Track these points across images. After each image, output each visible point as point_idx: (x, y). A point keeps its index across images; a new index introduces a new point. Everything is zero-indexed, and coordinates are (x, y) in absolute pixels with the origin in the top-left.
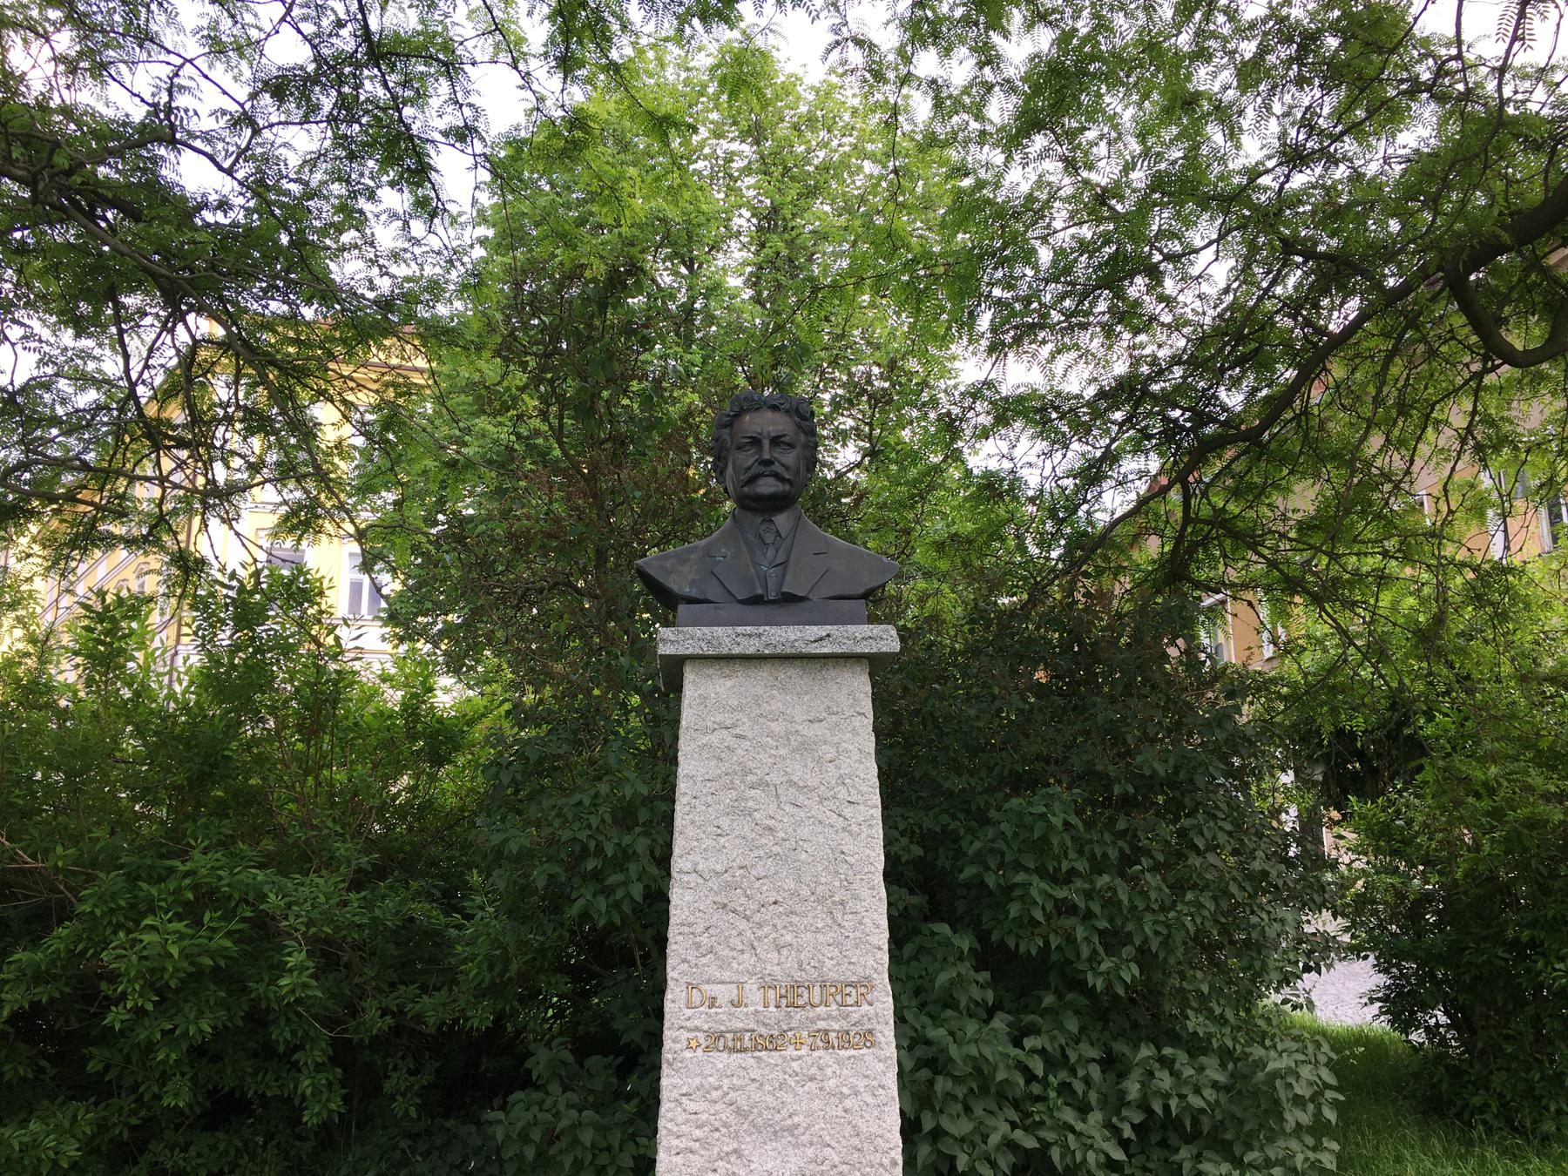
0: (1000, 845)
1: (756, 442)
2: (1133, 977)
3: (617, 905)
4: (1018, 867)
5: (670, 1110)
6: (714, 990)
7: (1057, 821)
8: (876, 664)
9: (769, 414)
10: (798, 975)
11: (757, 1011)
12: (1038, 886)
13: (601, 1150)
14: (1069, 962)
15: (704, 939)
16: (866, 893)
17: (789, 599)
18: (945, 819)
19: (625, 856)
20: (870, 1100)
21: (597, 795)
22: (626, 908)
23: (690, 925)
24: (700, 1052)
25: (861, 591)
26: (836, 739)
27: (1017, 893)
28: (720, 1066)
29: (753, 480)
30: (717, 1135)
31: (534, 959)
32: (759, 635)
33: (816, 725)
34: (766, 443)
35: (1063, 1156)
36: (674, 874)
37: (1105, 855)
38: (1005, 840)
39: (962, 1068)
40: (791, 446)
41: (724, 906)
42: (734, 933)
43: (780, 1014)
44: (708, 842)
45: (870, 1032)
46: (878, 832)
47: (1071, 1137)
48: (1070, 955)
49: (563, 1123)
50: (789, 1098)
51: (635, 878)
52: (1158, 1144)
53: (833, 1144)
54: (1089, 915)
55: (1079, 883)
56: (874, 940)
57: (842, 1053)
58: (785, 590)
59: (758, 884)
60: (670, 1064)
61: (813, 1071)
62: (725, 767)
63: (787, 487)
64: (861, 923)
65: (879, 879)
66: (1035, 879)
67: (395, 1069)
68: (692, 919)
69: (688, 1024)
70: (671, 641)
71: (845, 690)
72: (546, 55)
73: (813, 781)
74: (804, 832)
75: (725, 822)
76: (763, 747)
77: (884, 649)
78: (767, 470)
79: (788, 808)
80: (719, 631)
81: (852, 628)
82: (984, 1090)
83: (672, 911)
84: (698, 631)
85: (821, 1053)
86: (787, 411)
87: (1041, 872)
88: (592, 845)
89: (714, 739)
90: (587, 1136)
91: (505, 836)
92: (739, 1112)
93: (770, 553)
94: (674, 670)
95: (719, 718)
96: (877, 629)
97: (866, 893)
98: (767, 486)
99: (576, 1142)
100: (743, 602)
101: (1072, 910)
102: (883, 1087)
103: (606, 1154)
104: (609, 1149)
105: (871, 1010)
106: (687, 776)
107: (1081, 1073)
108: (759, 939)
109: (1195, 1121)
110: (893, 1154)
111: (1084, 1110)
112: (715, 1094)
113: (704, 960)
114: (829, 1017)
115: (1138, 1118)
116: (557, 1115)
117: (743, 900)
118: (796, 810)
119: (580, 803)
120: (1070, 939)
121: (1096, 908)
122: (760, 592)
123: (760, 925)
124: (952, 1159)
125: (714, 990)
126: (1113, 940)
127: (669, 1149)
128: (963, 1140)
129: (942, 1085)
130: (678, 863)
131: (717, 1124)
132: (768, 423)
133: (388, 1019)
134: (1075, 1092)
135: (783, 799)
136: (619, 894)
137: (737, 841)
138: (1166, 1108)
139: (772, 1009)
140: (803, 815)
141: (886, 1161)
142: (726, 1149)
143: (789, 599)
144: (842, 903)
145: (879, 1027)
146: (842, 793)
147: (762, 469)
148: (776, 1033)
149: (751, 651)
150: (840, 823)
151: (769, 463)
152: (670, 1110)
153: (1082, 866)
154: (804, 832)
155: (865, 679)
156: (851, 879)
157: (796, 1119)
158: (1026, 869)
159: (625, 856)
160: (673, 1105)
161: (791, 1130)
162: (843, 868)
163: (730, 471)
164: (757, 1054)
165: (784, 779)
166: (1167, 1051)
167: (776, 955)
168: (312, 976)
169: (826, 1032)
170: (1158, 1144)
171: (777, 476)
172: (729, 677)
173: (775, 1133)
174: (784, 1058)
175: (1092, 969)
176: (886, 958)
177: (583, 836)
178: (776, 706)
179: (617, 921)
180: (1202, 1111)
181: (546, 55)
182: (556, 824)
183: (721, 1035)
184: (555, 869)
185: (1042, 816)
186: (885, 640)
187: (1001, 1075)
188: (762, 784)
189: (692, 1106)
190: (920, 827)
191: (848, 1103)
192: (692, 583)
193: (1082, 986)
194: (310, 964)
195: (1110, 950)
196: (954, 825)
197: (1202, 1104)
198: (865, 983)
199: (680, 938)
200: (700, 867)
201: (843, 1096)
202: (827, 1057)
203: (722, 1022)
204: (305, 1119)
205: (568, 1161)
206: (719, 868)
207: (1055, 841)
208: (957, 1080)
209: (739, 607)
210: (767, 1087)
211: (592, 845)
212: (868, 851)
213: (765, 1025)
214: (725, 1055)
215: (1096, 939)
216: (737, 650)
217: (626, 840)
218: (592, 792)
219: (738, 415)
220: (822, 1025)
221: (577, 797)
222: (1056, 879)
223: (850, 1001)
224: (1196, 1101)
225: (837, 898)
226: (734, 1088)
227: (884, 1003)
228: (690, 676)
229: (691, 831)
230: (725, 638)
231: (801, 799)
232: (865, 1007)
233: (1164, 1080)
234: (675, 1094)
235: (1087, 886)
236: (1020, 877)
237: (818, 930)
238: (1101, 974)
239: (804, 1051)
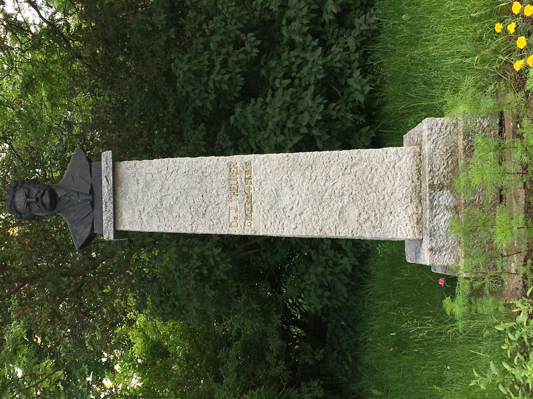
0: (197, 92)
1: (28, 204)
2: (254, 36)
3: (223, 259)
4: (206, 84)
5: (270, 232)
6: (232, 217)
7: (186, 68)
8: (116, 159)
9: (17, 199)
10: (227, 188)
11: (239, 203)
12: (215, 77)
13: (327, 264)
14: (247, 63)
15: (215, 221)
16: (199, 164)
17: (92, 191)
18: (188, 112)
19: (203, 258)
20: (268, 164)
21: (175, 270)
22: (224, 255)
23: (210, 226)
24: (252, 222)
25: (87, 163)
26: (144, 174)
27: (218, 85)
28: (256, 215)
29: (43, 205)
30: (278, 216)
31: (252, 298)
32: (106, 203)
33: (139, 181)
34: (28, 200)
35: (320, 74)
36: (192, 232)
37: (202, 44)
38: (196, 89)
39: (284, 116)
40: (29, 190)
41: (204, 214)
42: (213, 211)
43: (240, 194)
44: (182, 221)
45: (246, 163)
46: (178, 159)
47: (314, 70)
48: (244, 63)
49: (315, 280)
50: (267, 192)
51: (211, 252)
52: (323, 27)
53: (281, 177)
54: (228, 53)
55: (214, 57)
56: (215, 162)
57: (252, 173)
58: (88, 193)
59: (196, 202)
60: (256, 232)
61: (258, 183)
62: (155, 215)
63: (47, 192)
64: (209, 166)
65: (194, 159)
66: (212, 77)
67: (304, 360)
68: (208, 226)
69: (243, 226)
70: (108, 235)
71: (127, 171)
73: (160, 183)
74: (178, 186)
75: (175, 214)
76: (147, 200)
77: (111, 156)
78: (40, 200)
79: (169, 192)
80: (104, 217)
81: (103, 169)
82: (295, 105)
83: (205, 233)
84: (105, 225)
85: (252, 180)
86: (15, 192)
87: (209, 74)
88: (197, 271)
89: (145, 219)
90: (320, 269)
91: (193, 309)
92: (271, 209)
93: (73, 198)
94: (118, 233)
95: (137, 217)
96: (103, 159)
97: (199, 164)
98: (47, 199)
99: (323, 274)
100: (93, 209)
101: (225, 61)
103: (329, 262)
104: (326, 261)
106: (158, 228)
107: (293, 60)
108: (215, 202)
109: (313, 11)
110: (284, 156)
111: (305, 61)
112: (265, 217)
113: (222, 221)
114: (241, 178)
115: (310, 37)
116: (313, 283)
117: (202, 208)
118: (170, 189)
119: (179, 277)
120: (237, 63)
121: (224, 51)
122: (89, 202)
123: (210, 202)
124: (318, 121)
126: (238, 44)
127: (282, 232)
128: (311, 116)
129: (290, 124)
130: (189, 231)
131: (275, 216)
132: (20, 199)
133: (280, 362)
134: (301, 63)
135: (166, 193)
136: (218, 259)
137: (181, 210)
138: (307, 25)
139: (238, 197)
140: (172, 187)
141: (287, 159)
142: (282, 213)
143: (92, 191)
144: (203, 173)
145: (244, 161)
146: (164, 172)
147: (40, 202)
148: (246, 196)
149: (112, 205)
150: (175, 173)
151: (37, 199)
152: (270, 232)
153: (206, 55)
154: (178, 186)
155: (122, 163)
156: (194, 170)
157: (273, 189)
158: (208, 80)
159: (203, 258)
160: (268, 231)
161: (277, 191)
162: (190, 172)
163: (40, 214)
165: (159, 193)
166: (284, 22)
167: (220, 196)
168: (255, 391)
169: (245, 179)
170: (323, 27)
171: (42, 196)
172: (121, 214)
173: (278, 196)
174: (254, 193)
175: (250, 53)
176: (221, 157)
177: (192, 275)
178: (132, 196)
179: (229, 260)
180: (309, 8)
182: (187, 287)
183: (246, 215)
184: (207, 287)
185: (184, 73)
186: (107, 156)
187: (288, 99)
188: (161, 201)
189: (269, 224)
190: (191, 124)
191: (268, 171)
192: (86, 228)
193: (259, 58)
194: (250, 392)
195: (243, 45)
196: (191, 109)
197: (306, 8)
198: (229, 165)
199: (214, 229)
200: (190, 223)
202: (254, 178)
203: (242, 215)
204: (322, 396)
205: (330, 278)
206: (190, 216)
207: (195, 68)
208: (289, 117)
209: (95, 210)
211: (197, 271)
212: (185, 163)
213: (243, 200)
215: (237, 51)
216: (112, 211)
217: (195, 256)
218: (174, 272)
219: (16, 210)
220: (243, 180)
221: (176, 278)
222: (212, 66)
223: (236, 170)
224: (305, 11)
225: (201, 175)
226: (264, 210)
227: (238, 159)
228: (122, 228)
229: (178, 227)
230: (107, 216)
231: (167, 187)
233: (295, 25)
234: (265, 230)
235: (215, 54)
236: (211, 84)
237: (212, 181)
238: (252, 50)
239: (252, 186)
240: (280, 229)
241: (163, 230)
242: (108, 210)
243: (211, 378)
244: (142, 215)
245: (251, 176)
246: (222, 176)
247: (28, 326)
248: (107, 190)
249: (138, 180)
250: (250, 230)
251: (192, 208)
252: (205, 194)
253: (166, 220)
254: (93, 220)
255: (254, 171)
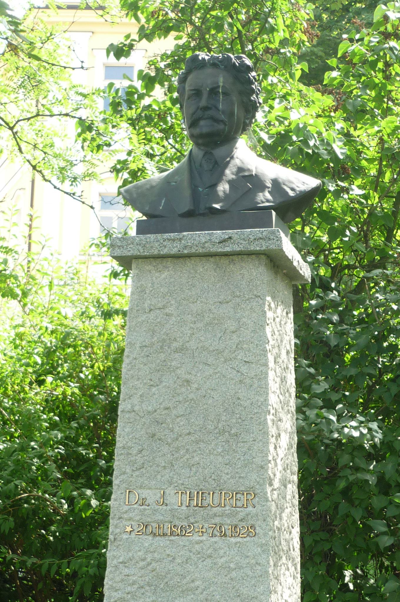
6: (145, 493)
24: (133, 535)
30: (143, 591)
32: (180, 240)
33: (224, 306)
50: (191, 568)
57: (233, 540)
72: (97, 315)
95: (154, 301)
102: (259, 564)
105: (254, 511)
125: (145, 493)
139: (184, 508)
149: (174, 251)
164: (172, 538)
181: (97, 315)
191: (234, 574)
200: (136, 408)
201: (230, 570)
210: (179, 561)
213: (179, 518)
214: (150, 538)
216: (165, 251)
220: (217, 520)
223: (239, 504)
232: (250, 508)
234: (115, 562)
240: (115, 594)
241: (273, 390)
242: (165, 243)
243: (69, 530)
244: (158, 311)
245: (225, 535)
246: (227, 474)
247: (308, 146)
248: (203, 240)
249: (228, 302)
250: (118, 530)
251: (166, 411)
252: (193, 438)
253: (145, 360)
254: (162, 217)
255: (236, 543)
